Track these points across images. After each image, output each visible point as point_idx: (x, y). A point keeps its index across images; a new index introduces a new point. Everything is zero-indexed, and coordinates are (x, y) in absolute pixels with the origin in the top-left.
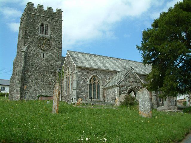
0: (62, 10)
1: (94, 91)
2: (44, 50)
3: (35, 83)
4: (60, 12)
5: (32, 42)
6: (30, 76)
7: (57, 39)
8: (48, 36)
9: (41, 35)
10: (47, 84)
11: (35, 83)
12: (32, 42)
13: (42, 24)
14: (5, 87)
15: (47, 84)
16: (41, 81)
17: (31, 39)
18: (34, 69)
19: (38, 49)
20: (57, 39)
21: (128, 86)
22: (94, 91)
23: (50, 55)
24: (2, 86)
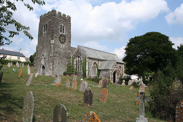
0: (70, 17)
1: (94, 71)
2: (62, 43)
3: (58, 63)
4: (69, 18)
5: (56, 37)
6: (56, 59)
7: (69, 36)
8: (64, 34)
9: (61, 33)
10: (64, 64)
11: (58, 63)
12: (56, 37)
13: (61, 25)
14: (6, 56)
15: (64, 64)
16: (61, 63)
17: (56, 35)
18: (58, 55)
19: (59, 42)
20: (69, 36)
21: (113, 70)
22: (94, 71)
23: (65, 46)
24: (4, 55)
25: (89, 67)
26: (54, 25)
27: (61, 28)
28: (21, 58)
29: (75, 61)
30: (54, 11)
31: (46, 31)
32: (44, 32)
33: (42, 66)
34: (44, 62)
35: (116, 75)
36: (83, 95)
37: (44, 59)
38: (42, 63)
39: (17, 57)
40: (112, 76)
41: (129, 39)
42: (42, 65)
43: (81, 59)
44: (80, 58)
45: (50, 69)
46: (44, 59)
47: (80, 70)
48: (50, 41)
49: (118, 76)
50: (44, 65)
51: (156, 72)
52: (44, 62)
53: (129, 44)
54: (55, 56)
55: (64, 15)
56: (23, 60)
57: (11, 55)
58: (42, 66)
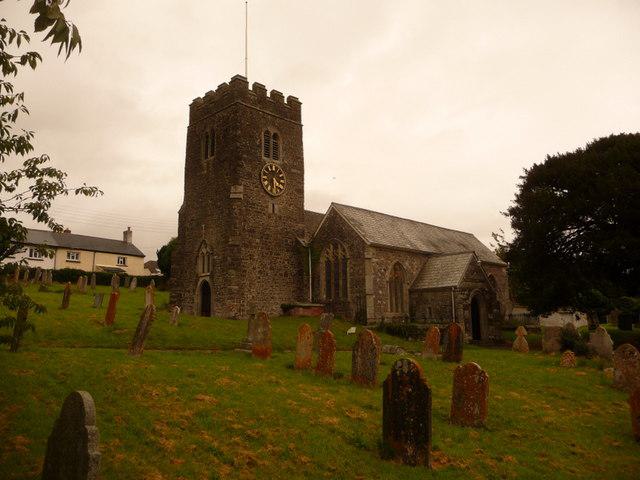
4: (294, 105)
6: (251, 257)
13: (267, 132)
21: (470, 290)
25: (374, 277)
26: (241, 134)
27: (267, 141)
28: (130, 260)
29: (323, 260)
30: (239, 82)
31: (212, 155)
32: (206, 158)
33: (199, 283)
34: (206, 270)
35: (483, 311)
36: (60, 409)
37: (206, 258)
38: (200, 270)
39: (116, 256)
40: (468, 313)
41: (515, 198)
42: (201, 280)
43: (344, 251)
44: (340, 251)
45: (231, 292)
46: (206, 258)
47: (341, 295)
48: (229, 191)
49: (491, 312)
50: (207, 279)
51: (592, 327)
52: (206, 270)
53: (525, 188)
54: (246, 246)
55: (276, 95)
56: (135, 268)
57: (96, 251)
58: (199, 283)
